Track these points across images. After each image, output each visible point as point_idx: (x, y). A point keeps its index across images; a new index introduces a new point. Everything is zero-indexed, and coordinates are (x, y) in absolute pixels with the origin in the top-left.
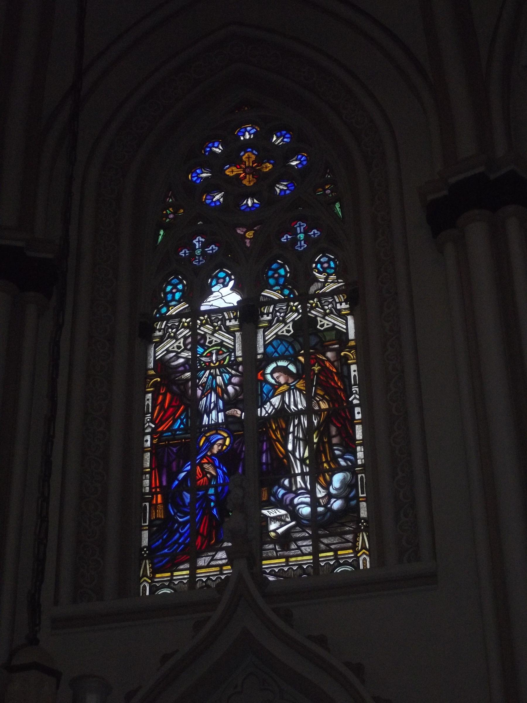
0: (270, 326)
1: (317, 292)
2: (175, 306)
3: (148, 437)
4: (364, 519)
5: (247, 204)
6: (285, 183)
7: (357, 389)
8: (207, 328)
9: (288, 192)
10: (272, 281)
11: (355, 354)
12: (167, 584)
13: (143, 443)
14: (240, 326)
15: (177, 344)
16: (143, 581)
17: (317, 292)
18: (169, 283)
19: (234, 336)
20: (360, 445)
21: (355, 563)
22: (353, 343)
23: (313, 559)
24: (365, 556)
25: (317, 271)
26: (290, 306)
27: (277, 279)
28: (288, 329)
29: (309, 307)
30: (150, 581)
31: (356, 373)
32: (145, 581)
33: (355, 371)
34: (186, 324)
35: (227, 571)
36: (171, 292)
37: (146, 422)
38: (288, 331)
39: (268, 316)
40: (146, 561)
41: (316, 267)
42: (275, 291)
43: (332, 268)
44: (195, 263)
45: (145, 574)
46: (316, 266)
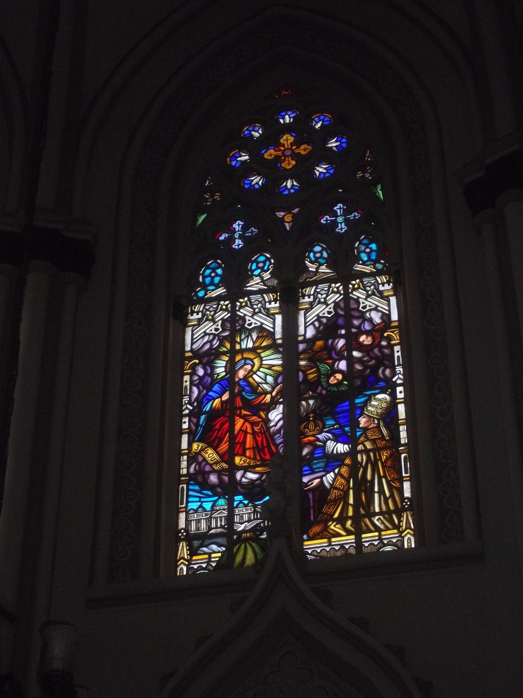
0: (199, 325)
2: (213, 290)
3: (186, 419)
4: (407, 498)
5: (286, 186)
6: (325, 166)
7: (401, 370)
8: (361, 293)
9: (327, 175)
10: (364, 257)
11: (398, 334)
12: (214, 565)
13: (182, 425)
14: (394, 289)
15: (327, 309)
16: (180, 564)
17: (307, 280)
18: (208, 267)
19: (389, 302)
20: (403, 424)
21: (399, 543)
22: (396, 324)
23: (356, 539)
24: (409, 536)
25: (309, 260)
26: (331, 287)
27: (369, 254)
29: (239, 306)
30: (187, 563)
31: (399, 354)
33: (398, 352)
34: (224, 307)
36: (209, 275)
37: (184, 404)
38: (329, 313)
40: (183, 543)
43: (324, 258)
44: (338, 231)
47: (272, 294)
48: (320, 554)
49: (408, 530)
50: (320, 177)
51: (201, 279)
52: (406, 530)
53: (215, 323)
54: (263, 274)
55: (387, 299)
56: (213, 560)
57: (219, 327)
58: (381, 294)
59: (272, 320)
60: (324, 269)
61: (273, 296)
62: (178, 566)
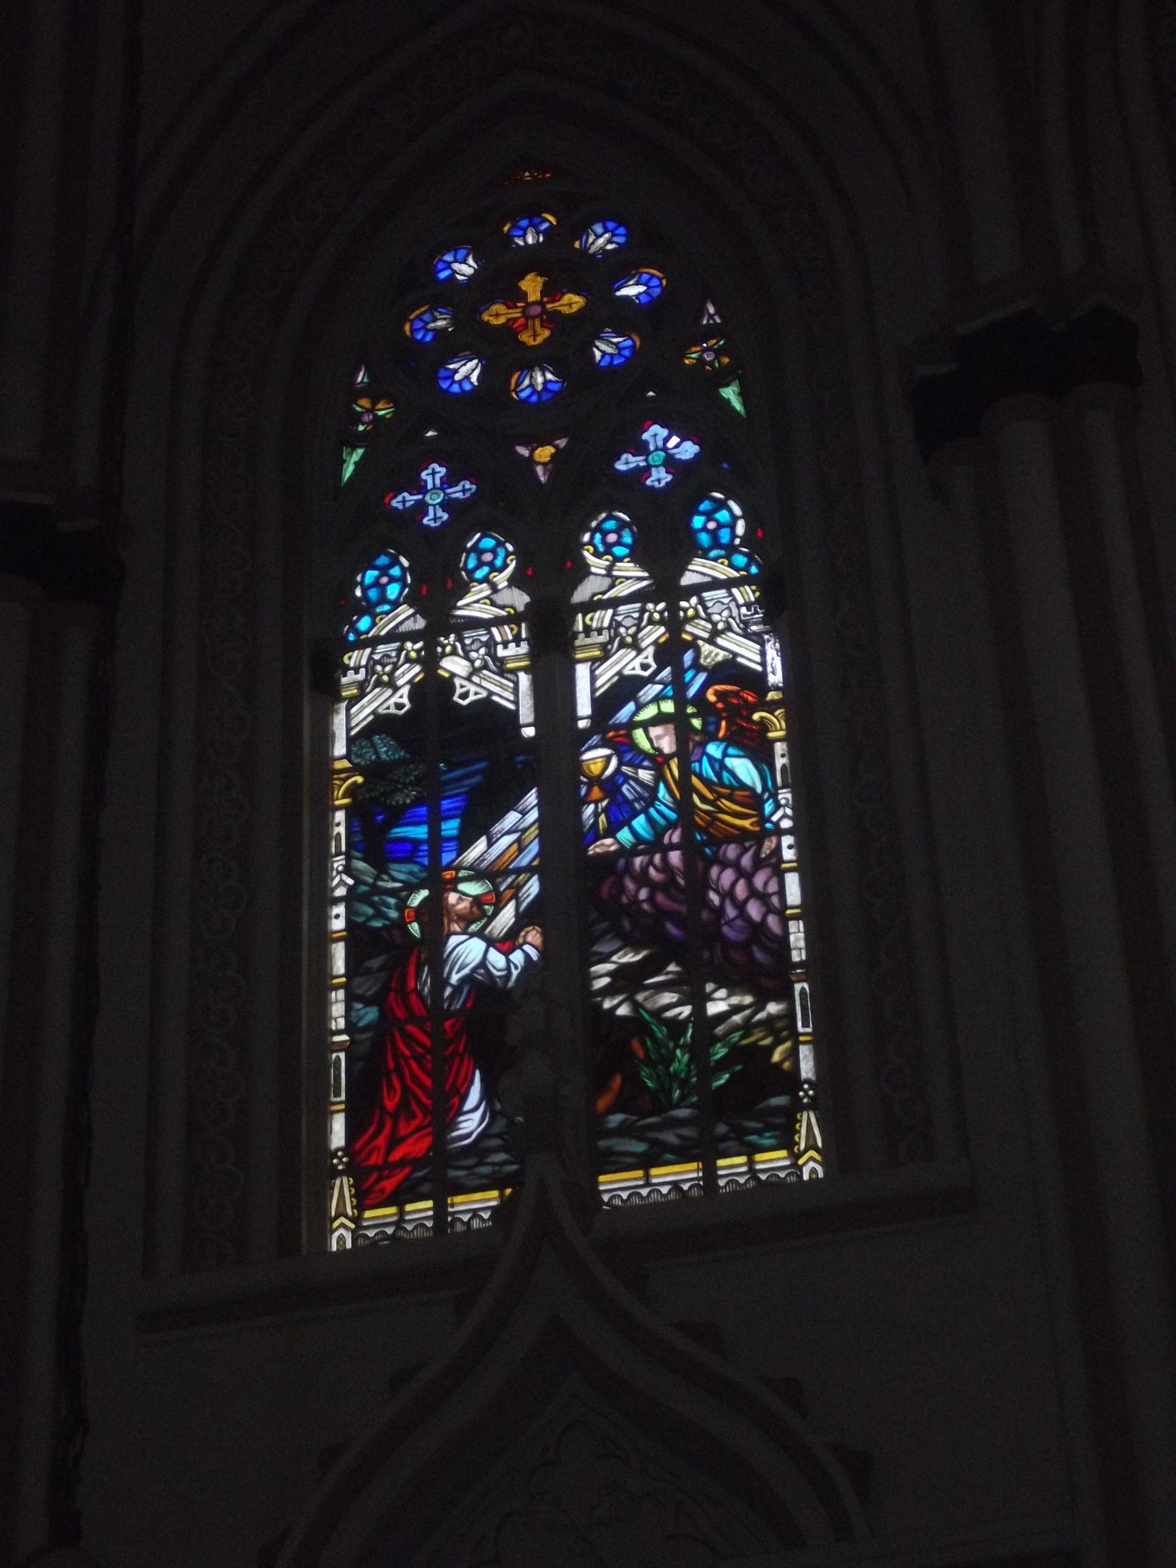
0: (606, 656)
1: (595, 598)
2: (387, 613)
3: (340, 909)
4: (807, 1081)
7: (789, 796)
10: (704, 538)
11: (784, 717)
15: (395, 699)
16: (338, 1228)
17: (595, 598)
20: (795, 917)
23: (434, 1208)
24: (812, 1164)
26: (646, 611)
28: (645, 661)
30: (353, 1226)
32: (343, 1225)
35: (371, 1221)
36: (376, 583)
38: (399, 706)
39: (600, 634)
41: (591, 542)
42: (715, 559)
45: (811, 1142)
46: (592, 538)
47: (508, 625)
48: (726, 1189)
49: (342, 1220)
50: (602, 364)
51: (358, 593)
52: (806, 1151)
53: (640, 651)
54: (495, 577)
55: (757, 638)
56: (408, 1218)
57: (651, 661)
58: (502, 668)
59: (511, 685)
60: (631, 569)
61: (512, 630)
62: (333, 1231)
